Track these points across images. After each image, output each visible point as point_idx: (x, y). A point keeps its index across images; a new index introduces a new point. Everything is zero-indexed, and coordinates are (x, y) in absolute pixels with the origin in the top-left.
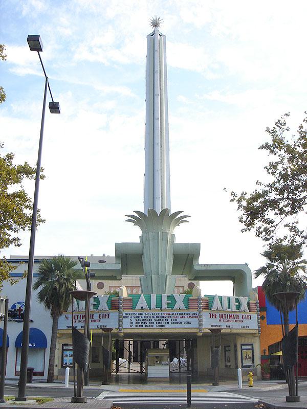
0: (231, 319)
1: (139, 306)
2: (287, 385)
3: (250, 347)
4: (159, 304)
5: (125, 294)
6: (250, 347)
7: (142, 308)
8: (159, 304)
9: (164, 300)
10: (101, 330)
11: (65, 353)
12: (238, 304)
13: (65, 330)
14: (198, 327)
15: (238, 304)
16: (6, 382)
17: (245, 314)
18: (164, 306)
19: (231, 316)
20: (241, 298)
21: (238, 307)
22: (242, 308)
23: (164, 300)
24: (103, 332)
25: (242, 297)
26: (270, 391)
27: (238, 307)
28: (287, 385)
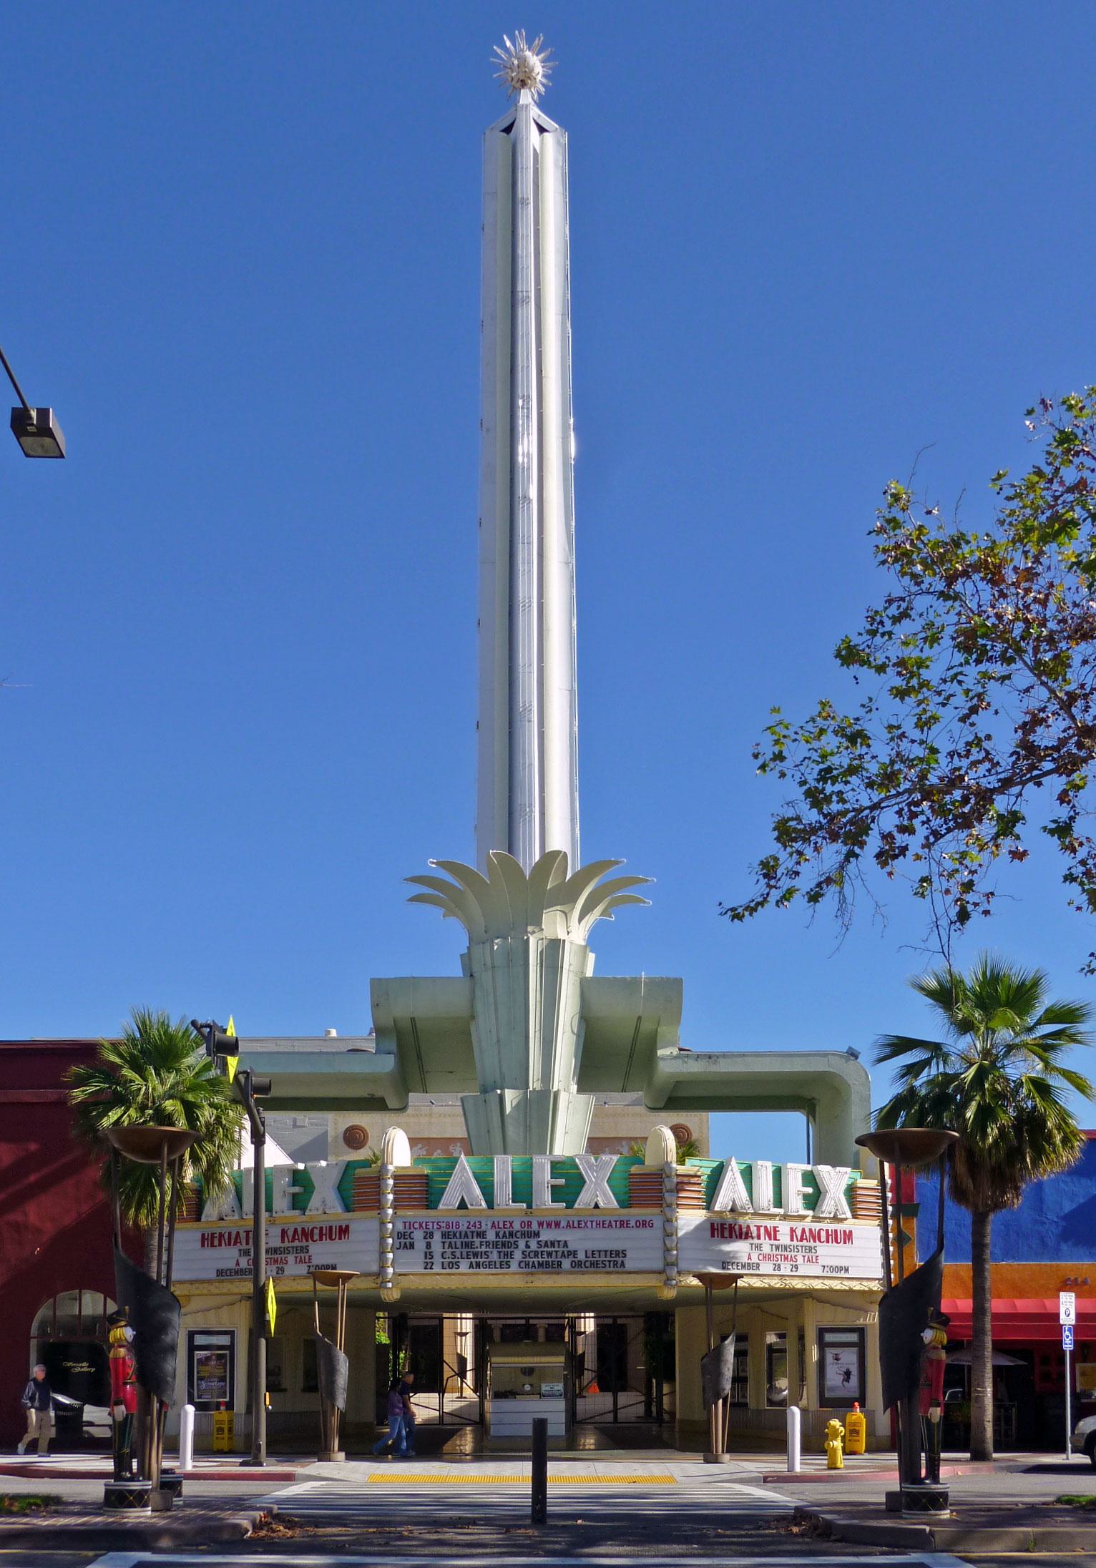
0: (296, 1243)
1: (449, 1200)
2: (895, 1456)
3: (854, 1337)
4: (523, 1189)
5: (400, 1155)
6: (854, 1337)
7: (463, 1205)
8: (523, 1189)
9: (544, 1177)
10: (311, 1282)
11: (199, 1354)
12: (810, 1190)
13: (209, 1281)
14: (659, 1265)
15: (810, 1190)
16: (560, 1387)
17: (799, 1226)
18: (544, 1199)
19: (557, 1224)
20: (824, 1171)
21: (813, 1201)
22: (827, 1207)
23: (544, 1177)
24: (319, 1286)
25: (828, 1168)
26: (564, 1526)
27: (813, 1201)
28: (895, 1456)
